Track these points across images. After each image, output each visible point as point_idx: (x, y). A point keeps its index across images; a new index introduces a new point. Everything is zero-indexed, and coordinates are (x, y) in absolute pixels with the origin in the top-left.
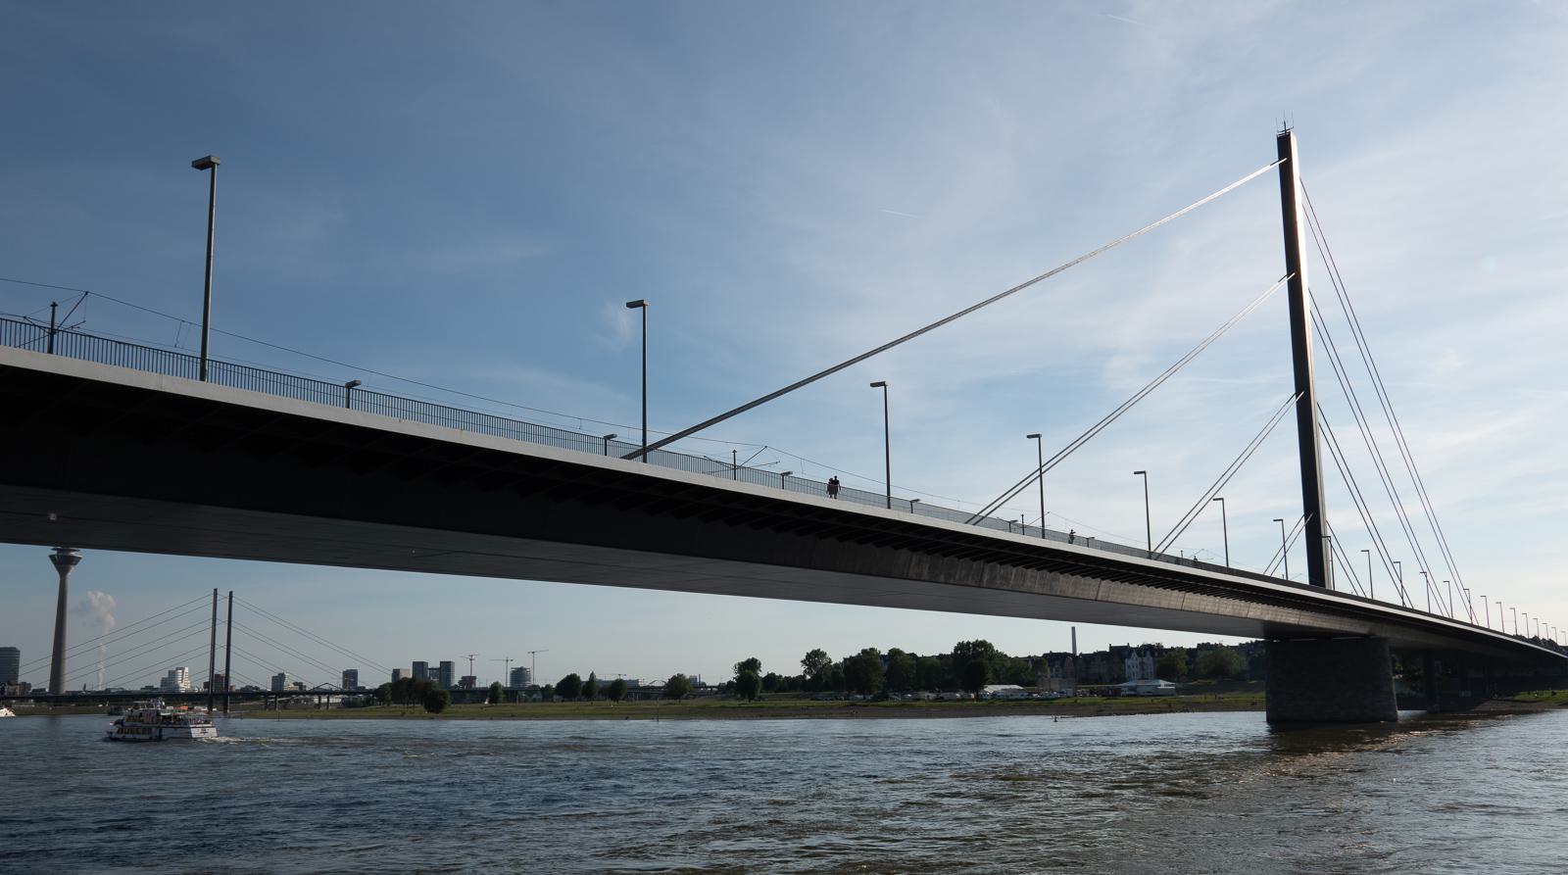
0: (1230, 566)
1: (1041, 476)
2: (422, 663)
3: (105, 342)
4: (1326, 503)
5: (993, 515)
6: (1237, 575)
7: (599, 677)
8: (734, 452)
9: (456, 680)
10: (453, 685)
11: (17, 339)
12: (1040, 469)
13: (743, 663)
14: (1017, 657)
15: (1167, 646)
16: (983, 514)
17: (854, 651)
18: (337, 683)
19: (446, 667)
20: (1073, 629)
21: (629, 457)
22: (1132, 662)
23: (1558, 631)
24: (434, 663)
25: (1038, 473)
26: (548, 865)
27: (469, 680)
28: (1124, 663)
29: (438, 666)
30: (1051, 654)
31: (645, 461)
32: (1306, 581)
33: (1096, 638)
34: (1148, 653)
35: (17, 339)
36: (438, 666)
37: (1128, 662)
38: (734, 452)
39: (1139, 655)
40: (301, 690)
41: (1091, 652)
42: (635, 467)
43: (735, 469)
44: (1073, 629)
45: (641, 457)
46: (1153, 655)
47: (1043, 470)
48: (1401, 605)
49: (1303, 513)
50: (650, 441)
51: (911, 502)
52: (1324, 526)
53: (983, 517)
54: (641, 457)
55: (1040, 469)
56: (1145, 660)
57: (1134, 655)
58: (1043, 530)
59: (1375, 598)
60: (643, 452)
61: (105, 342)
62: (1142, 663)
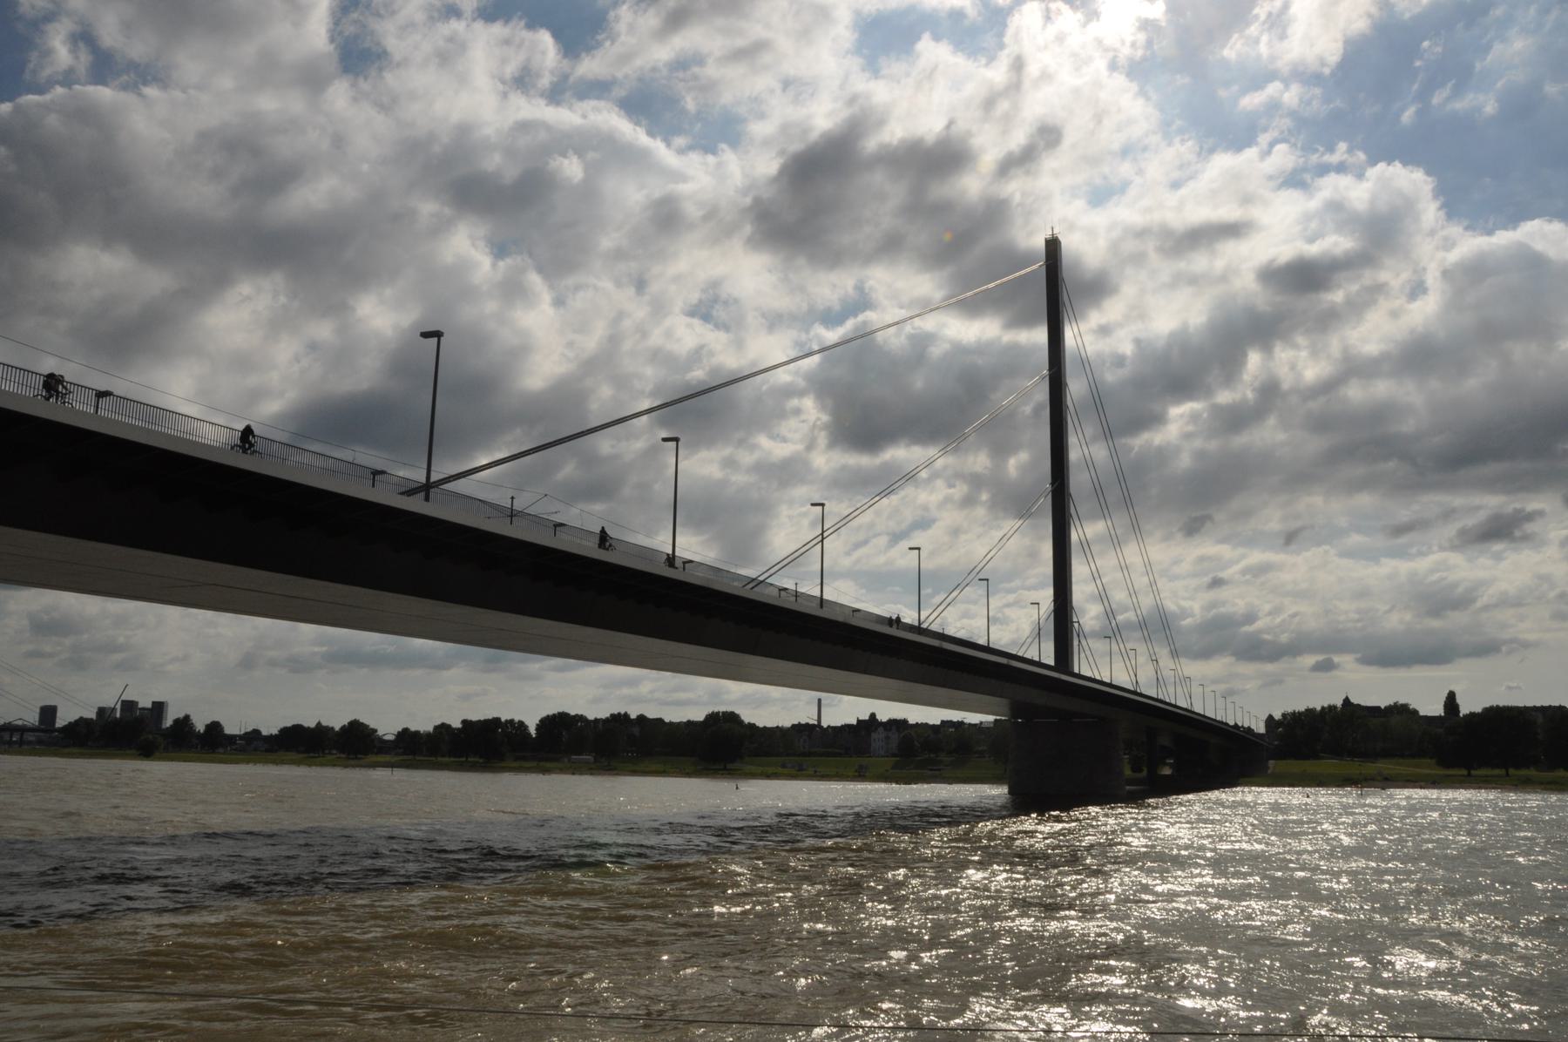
1: (822, 541)
2: (132, 702)
6: (999, 656)
7: (1354, 700)
8: (512, 498)
9: (168, 722)
10: (164, 727)
12: (822, 534)
13: (645, 717)
15: (912, 721)
16: (761, 578)
17: (345, 722)
18: (33, 718)
19: (159, 707)
20: (820, 701)
21: (410, 492)
22: (877, 737)
24: (145, 702)
25: (825, 534)
26: (1530, 944)
27: (214, 728)
29: (150, 706)
31: (427, 499)
32: (1051, 661)
33: (845, 710)
34: (894, 728)
36: (150, 706)
37: (874, 736)
38: (512, 498)
39: (885, 729)
42: (415, 505)
44: (820, 701)
45: (422, 495)
47: (820, 538)
48: (1156, 697)
49: (1052, 598)
52: (1072, 613)
53: (762, 582)
54: (422, 495)
55: (822, 534)
57: (881, 729)
59: (1178, 704)
62: (887, 738)
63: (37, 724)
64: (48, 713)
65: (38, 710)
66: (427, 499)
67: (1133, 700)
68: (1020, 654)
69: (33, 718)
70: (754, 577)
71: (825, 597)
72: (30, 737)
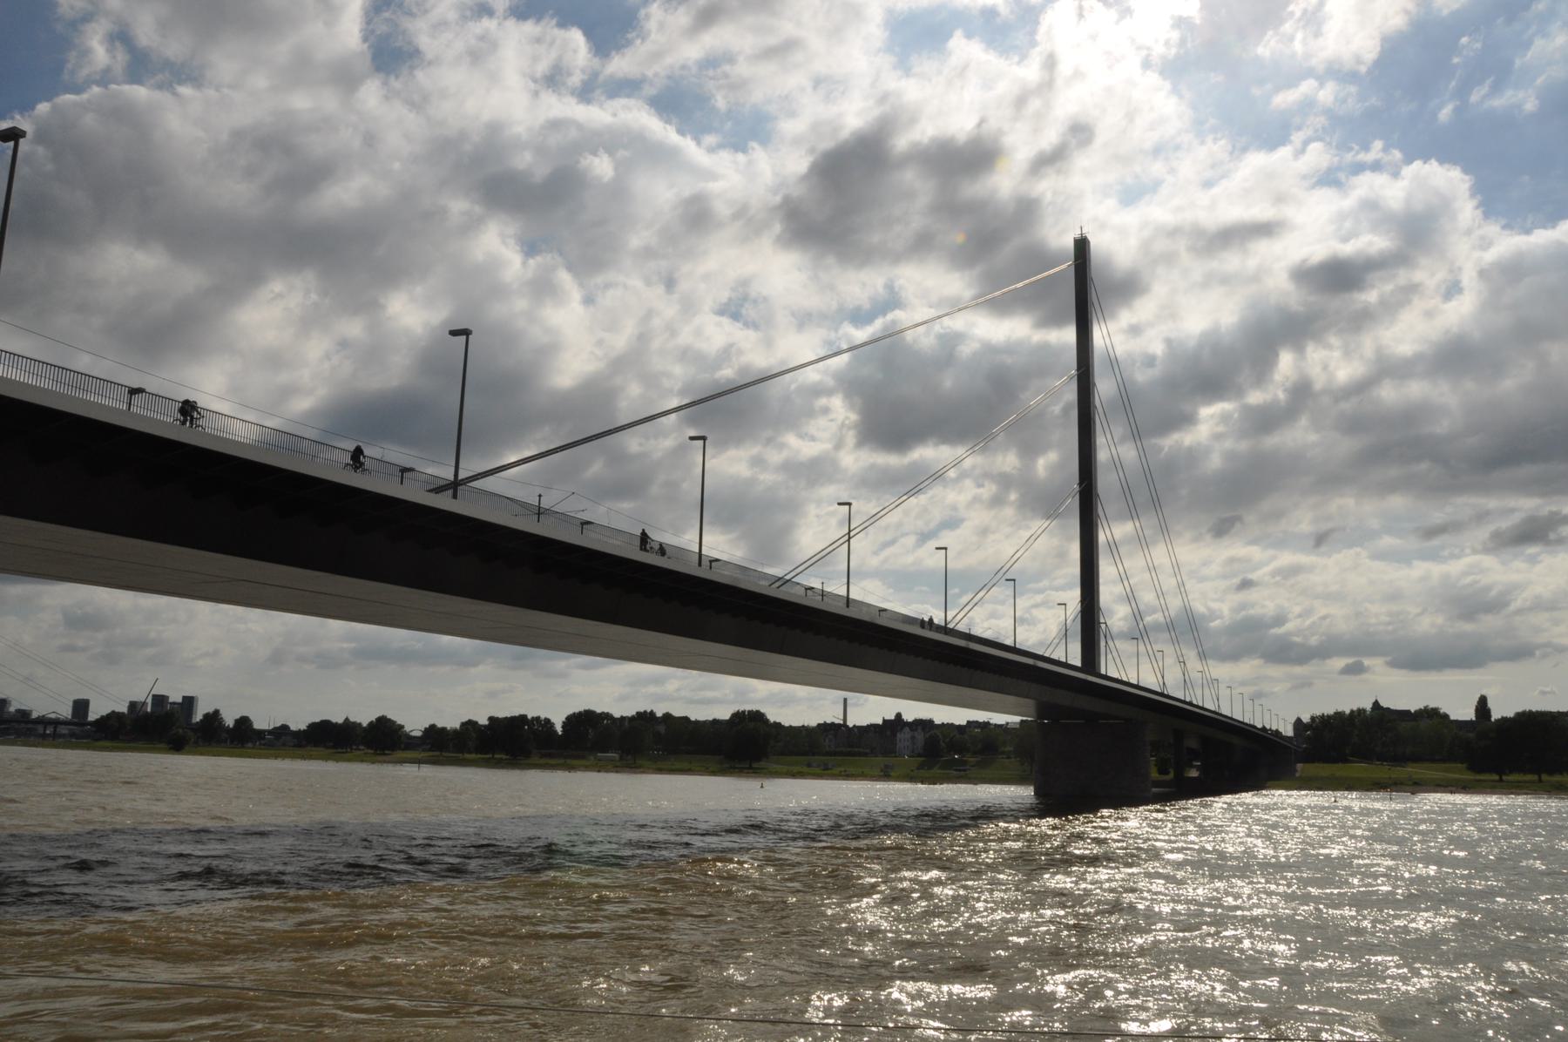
0: (1069, 662)
2: (163, 696)
3: (72, 373)
4: (1101, 581)
5: (793, 580)
8: (540, 496)
9: (198, 717)
11: (20, 364)
14: (791, 726)
15: (937, 722)
16: (788, 577)
18: (66, 712)
20: (845, 700)
21: (438, 490)
22: (903, 737)
23: (1273, 713)
24: (175, 697)
28: (896, 736)
29: (180, 700)
30: (825, 724)
31: (455, 496)
32: (1078, 663)
34: (920, 728)
35: (20, 364)
36: (180, 700)
38: (540, 496)
40: (24, 715)
41: (864, 723)
42: (444, 502)
43: (539, 514)
44: (845, 700)
45: (450, 492)
46: (923, 729)
48: (1183, 699)
50: (462, 475)
51: (806, 589)
53: (788, 581)
54: (450, 492)
55: (850, 538)
56: (916, 734)
58: (539, 508)
59: (1141, 684)
60: (455, 486)
61: (25, 359)
62: (913, 738)
63: (70, 717)
64: (81, 706)
65: (71, 704)
66: (455, 496)
67: (1203, 715)
68: (1047, 655)
69: (66, 712)
70: (780, 576)
71: (825, 589)
72: (63, 730)
